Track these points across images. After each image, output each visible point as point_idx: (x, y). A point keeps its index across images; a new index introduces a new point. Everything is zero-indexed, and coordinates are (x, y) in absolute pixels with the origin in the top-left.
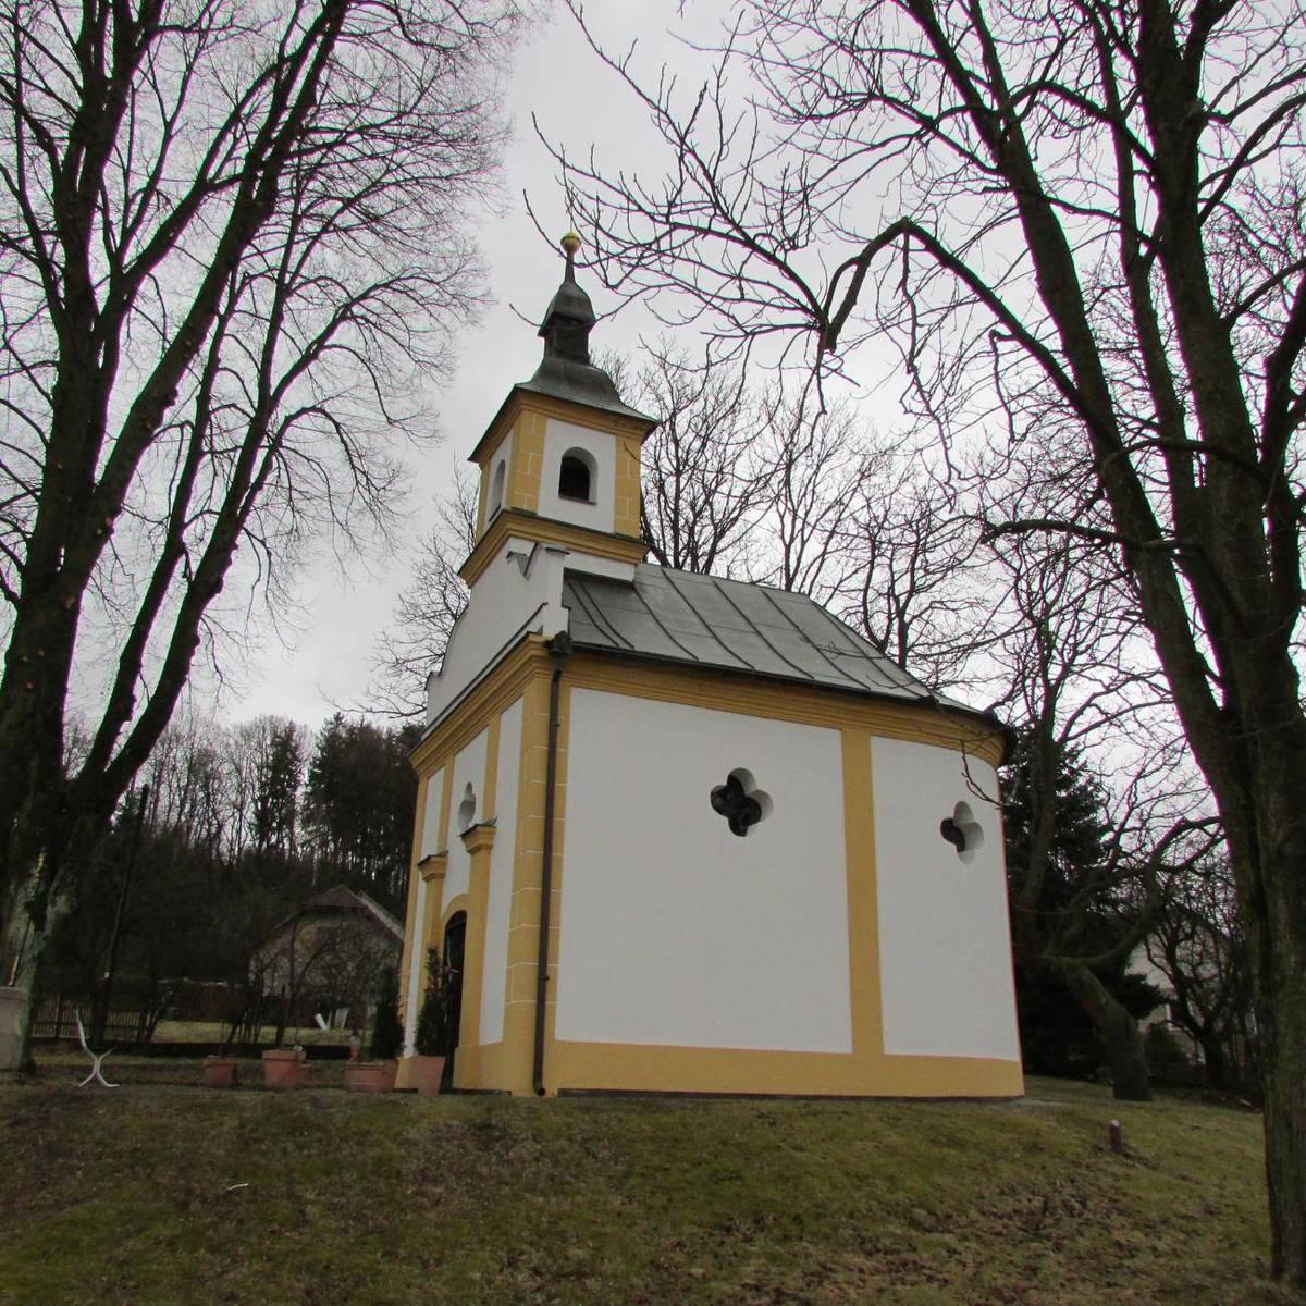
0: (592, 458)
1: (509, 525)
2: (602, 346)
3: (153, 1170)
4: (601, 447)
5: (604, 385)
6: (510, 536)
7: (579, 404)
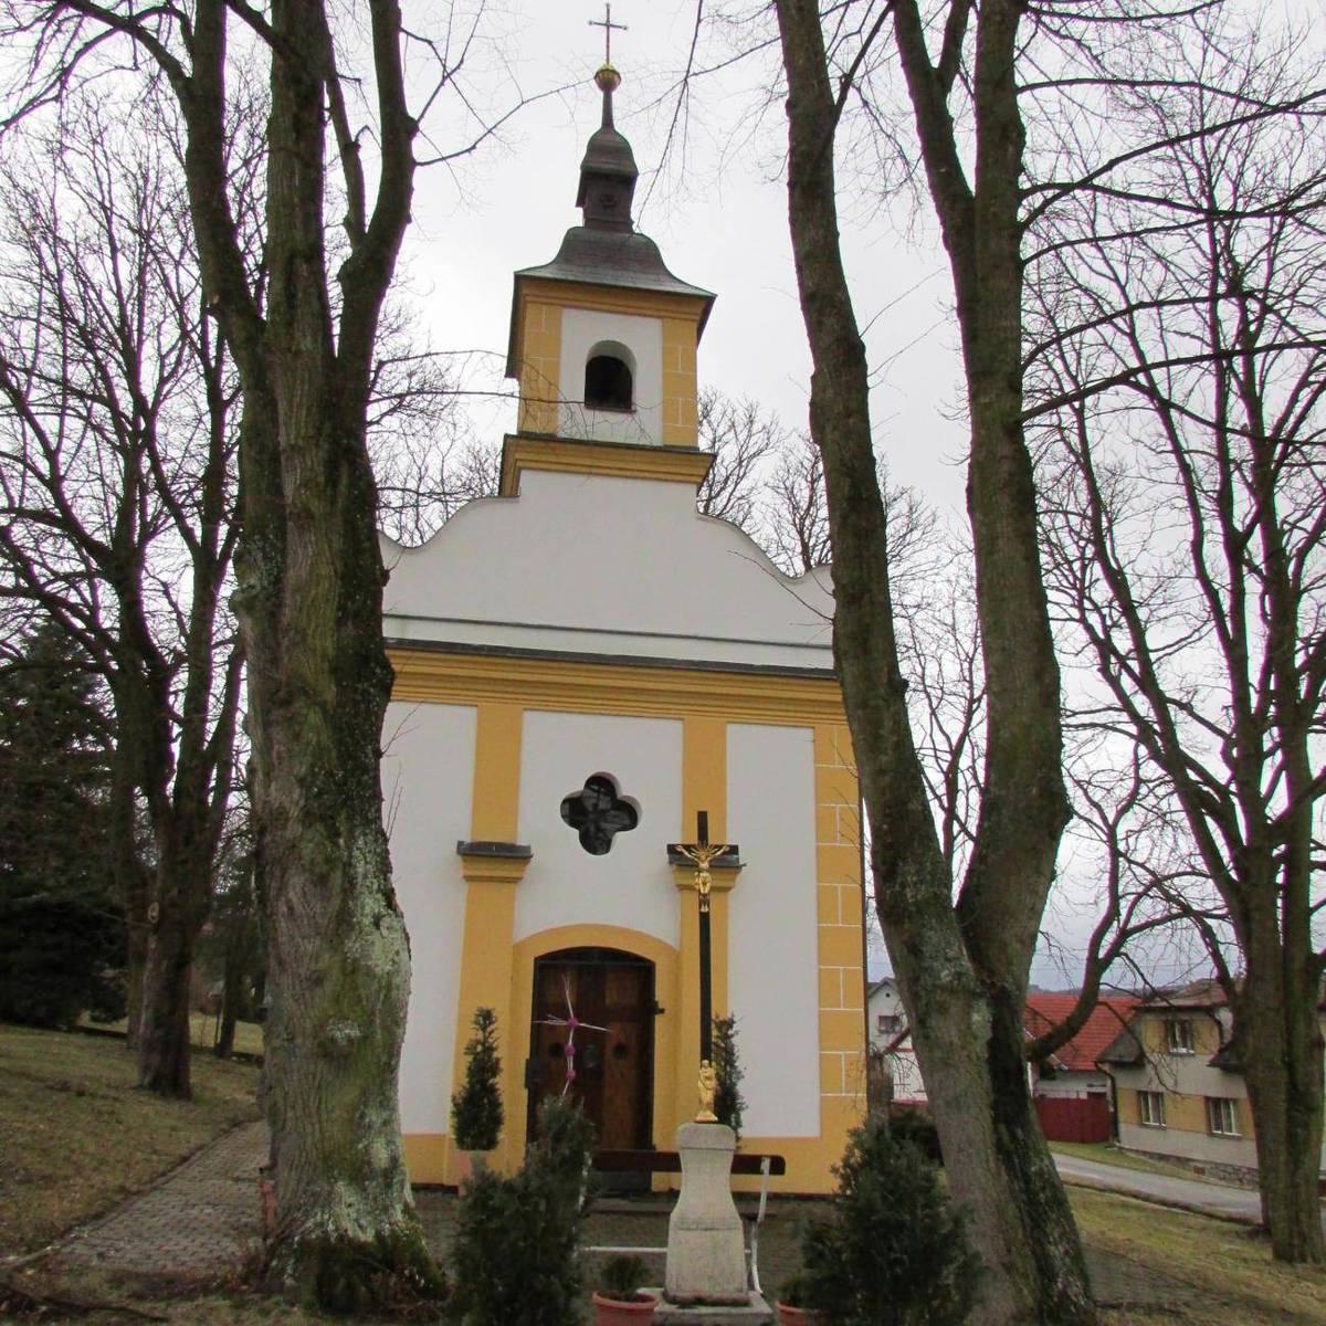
0: (624, 347)
1: (517, 456)
2: (647, 215)
3: (125, 1199)
4: (641, 339)
5: (648, 255)
6: (520, 469)
7: (624, 288)
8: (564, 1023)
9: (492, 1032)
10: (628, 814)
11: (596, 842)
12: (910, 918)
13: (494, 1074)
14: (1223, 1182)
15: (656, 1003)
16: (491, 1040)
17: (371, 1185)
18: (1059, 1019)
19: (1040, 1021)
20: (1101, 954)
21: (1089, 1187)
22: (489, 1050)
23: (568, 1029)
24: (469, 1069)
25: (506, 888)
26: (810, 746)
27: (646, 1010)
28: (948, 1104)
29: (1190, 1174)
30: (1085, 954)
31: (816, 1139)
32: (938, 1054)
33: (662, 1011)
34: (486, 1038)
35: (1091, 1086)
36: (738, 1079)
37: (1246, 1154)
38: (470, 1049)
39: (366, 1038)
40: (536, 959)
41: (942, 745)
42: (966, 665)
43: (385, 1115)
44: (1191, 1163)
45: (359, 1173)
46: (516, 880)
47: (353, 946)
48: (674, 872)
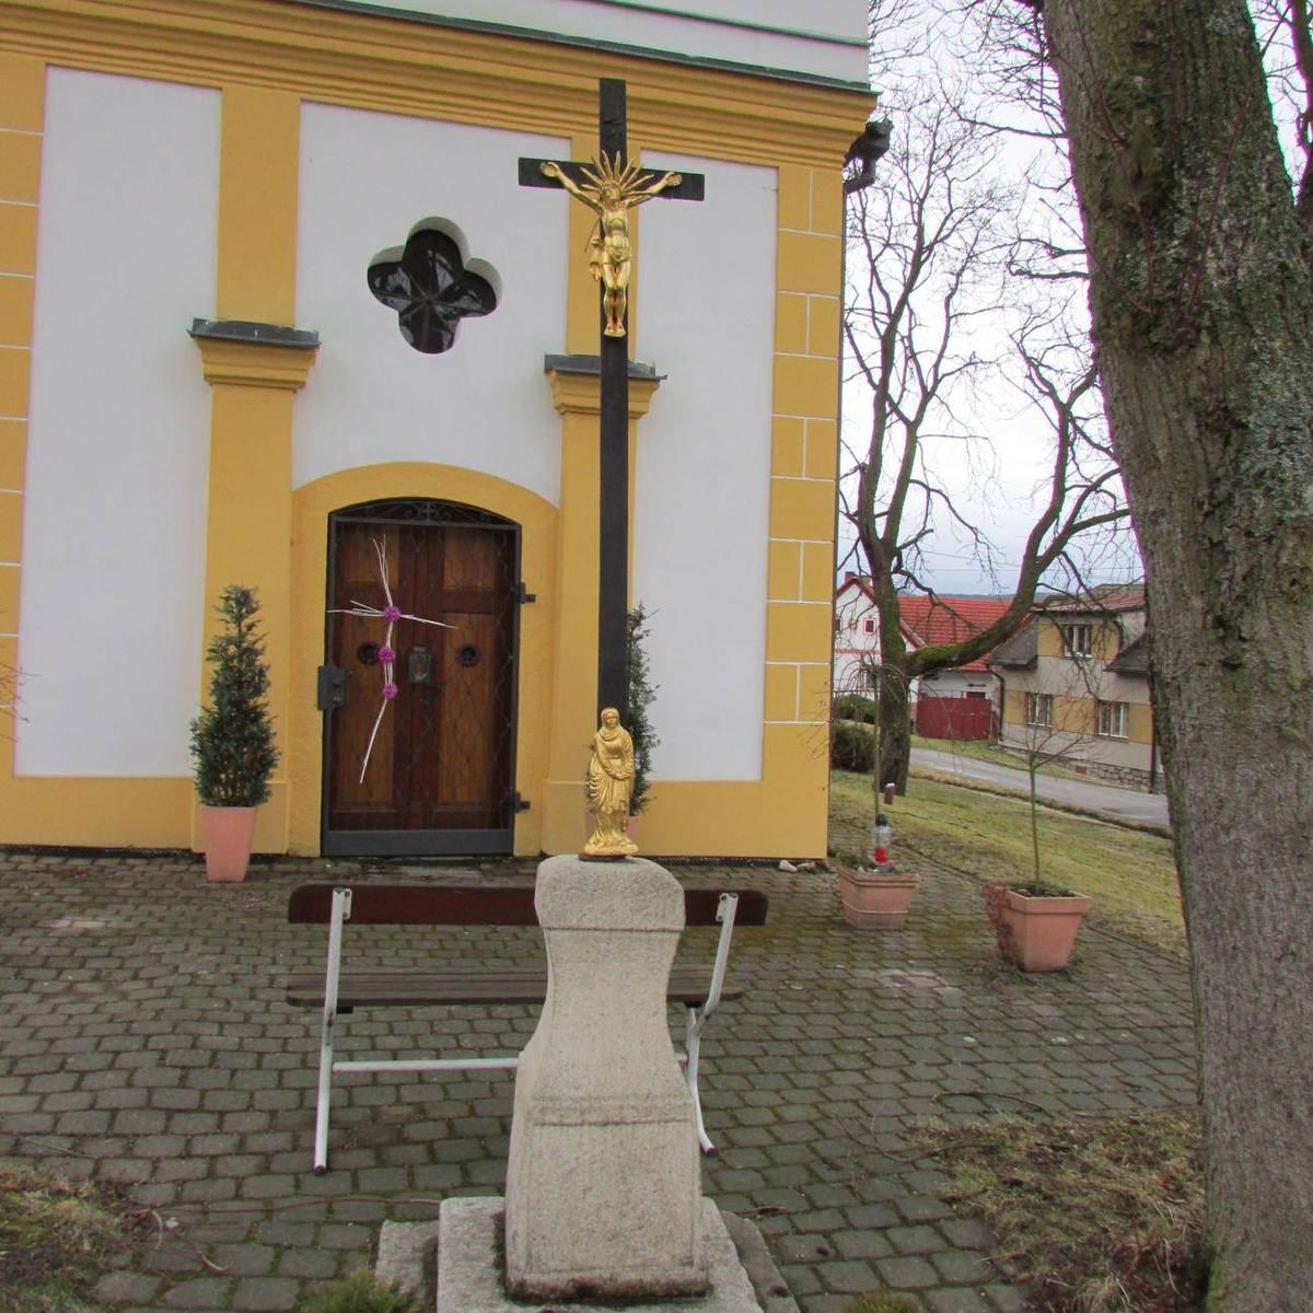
8: (378, 614)
9: (250, 627)
10: (479, 292)
11: (429, 333)
12: (1213, 332)
13: (258, 691)
14: (1104, 782)
15: (521, 587)
16: (250, 638)
18: (988, 622)
19: (960, 624)
20: (1041, 552)
21: (1014, 796)
22: (249, 653)
23: (385, 621)
24: (216, 682)
25: (276, 397)
26: (772, 196)
27: (507, 597)
28: (1271, 839)
29: (1072, 773)
30: (1022, 550)
32: (1262, 711)
33: (531, 599)
34: (242, 636)
35: (971, 685)
36: (646, 701)
37: (1138, 755)
38: (216, 652)
40: (330, 514)
41: (881, 306)
42: (916, 208)
44: (1072, 763)
46: (294, 387)
48: (553, 385)
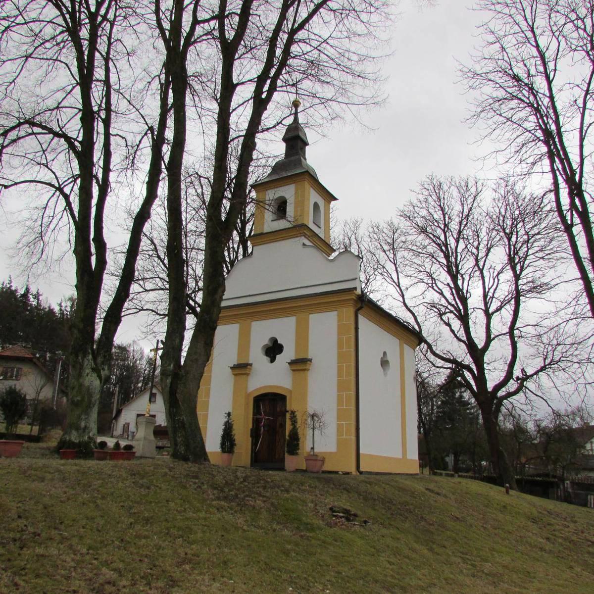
17: (80, 431)
31: (401, 459)
39: (83, 400)
43: (87, 417)
45: (78, 428)
47: (81, 380)
